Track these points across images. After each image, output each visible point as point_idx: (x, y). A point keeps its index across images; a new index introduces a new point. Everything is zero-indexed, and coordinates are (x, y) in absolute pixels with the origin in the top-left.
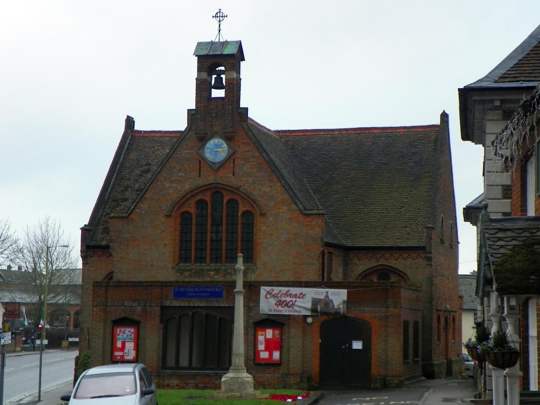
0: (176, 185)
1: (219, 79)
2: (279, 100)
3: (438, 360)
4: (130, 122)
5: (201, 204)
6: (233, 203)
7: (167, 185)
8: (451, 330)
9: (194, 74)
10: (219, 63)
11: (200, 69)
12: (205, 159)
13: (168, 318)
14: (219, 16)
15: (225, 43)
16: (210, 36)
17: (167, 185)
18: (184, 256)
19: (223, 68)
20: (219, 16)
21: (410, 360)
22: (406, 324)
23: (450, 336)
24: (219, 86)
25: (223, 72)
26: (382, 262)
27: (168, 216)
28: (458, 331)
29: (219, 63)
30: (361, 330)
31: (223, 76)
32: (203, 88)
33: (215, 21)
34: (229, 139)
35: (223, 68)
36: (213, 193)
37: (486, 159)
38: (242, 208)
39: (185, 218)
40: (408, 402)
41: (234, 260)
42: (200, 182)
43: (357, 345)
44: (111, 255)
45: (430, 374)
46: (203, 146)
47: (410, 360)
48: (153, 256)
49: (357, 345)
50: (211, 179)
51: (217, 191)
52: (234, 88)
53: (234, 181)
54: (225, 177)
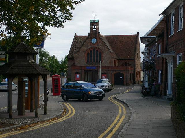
0: (86, 47)
1: (94, 27)
2: (104, 31)
3: (136, 80)
4: (75, 34)
5: (91, 51)
6: (97, 51)
7: (85, 47)
8: (139, 75)
9: (90, 26)
10: (94, 24)
11: (91, 25)
12: (92, 43)
13: (86, 72)
14: (95, 15)
15: (95, 20)
16: (94, 19)
17: (85, 47)
18: (88, 61)
19: (95, 25)
20: (95, 15)
21: (131, 80)
22: (130, 74)
23: (139, 76)
24: (94, 28)
25: (95, 26)
26: (126, 62)
27: (85, 53)
28: (140, 75)
29: (94, 24)
30: (122, 75)
31: (95, 26)
32: (91, 29)
33: (94, 16)
34: (96, 39)
35: (95, 25)
36: (93, 49)
37: (98, 31)
38: (99, 52)
39: (88, 54)
40: (27, 88)
41: (100, 62)
42: (91, 47)
43: (121, 78)
44: (74, 61)
45: (134, 83)
46: (91, 40)
47: (131, 80)
48: (82, 60)
49: (121, 78)
50: (93, 46)
51: (94, 48)
52: (97, 29)
53: (98, 47)
54: (96, 46)
